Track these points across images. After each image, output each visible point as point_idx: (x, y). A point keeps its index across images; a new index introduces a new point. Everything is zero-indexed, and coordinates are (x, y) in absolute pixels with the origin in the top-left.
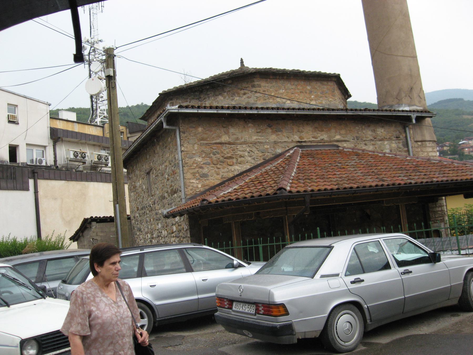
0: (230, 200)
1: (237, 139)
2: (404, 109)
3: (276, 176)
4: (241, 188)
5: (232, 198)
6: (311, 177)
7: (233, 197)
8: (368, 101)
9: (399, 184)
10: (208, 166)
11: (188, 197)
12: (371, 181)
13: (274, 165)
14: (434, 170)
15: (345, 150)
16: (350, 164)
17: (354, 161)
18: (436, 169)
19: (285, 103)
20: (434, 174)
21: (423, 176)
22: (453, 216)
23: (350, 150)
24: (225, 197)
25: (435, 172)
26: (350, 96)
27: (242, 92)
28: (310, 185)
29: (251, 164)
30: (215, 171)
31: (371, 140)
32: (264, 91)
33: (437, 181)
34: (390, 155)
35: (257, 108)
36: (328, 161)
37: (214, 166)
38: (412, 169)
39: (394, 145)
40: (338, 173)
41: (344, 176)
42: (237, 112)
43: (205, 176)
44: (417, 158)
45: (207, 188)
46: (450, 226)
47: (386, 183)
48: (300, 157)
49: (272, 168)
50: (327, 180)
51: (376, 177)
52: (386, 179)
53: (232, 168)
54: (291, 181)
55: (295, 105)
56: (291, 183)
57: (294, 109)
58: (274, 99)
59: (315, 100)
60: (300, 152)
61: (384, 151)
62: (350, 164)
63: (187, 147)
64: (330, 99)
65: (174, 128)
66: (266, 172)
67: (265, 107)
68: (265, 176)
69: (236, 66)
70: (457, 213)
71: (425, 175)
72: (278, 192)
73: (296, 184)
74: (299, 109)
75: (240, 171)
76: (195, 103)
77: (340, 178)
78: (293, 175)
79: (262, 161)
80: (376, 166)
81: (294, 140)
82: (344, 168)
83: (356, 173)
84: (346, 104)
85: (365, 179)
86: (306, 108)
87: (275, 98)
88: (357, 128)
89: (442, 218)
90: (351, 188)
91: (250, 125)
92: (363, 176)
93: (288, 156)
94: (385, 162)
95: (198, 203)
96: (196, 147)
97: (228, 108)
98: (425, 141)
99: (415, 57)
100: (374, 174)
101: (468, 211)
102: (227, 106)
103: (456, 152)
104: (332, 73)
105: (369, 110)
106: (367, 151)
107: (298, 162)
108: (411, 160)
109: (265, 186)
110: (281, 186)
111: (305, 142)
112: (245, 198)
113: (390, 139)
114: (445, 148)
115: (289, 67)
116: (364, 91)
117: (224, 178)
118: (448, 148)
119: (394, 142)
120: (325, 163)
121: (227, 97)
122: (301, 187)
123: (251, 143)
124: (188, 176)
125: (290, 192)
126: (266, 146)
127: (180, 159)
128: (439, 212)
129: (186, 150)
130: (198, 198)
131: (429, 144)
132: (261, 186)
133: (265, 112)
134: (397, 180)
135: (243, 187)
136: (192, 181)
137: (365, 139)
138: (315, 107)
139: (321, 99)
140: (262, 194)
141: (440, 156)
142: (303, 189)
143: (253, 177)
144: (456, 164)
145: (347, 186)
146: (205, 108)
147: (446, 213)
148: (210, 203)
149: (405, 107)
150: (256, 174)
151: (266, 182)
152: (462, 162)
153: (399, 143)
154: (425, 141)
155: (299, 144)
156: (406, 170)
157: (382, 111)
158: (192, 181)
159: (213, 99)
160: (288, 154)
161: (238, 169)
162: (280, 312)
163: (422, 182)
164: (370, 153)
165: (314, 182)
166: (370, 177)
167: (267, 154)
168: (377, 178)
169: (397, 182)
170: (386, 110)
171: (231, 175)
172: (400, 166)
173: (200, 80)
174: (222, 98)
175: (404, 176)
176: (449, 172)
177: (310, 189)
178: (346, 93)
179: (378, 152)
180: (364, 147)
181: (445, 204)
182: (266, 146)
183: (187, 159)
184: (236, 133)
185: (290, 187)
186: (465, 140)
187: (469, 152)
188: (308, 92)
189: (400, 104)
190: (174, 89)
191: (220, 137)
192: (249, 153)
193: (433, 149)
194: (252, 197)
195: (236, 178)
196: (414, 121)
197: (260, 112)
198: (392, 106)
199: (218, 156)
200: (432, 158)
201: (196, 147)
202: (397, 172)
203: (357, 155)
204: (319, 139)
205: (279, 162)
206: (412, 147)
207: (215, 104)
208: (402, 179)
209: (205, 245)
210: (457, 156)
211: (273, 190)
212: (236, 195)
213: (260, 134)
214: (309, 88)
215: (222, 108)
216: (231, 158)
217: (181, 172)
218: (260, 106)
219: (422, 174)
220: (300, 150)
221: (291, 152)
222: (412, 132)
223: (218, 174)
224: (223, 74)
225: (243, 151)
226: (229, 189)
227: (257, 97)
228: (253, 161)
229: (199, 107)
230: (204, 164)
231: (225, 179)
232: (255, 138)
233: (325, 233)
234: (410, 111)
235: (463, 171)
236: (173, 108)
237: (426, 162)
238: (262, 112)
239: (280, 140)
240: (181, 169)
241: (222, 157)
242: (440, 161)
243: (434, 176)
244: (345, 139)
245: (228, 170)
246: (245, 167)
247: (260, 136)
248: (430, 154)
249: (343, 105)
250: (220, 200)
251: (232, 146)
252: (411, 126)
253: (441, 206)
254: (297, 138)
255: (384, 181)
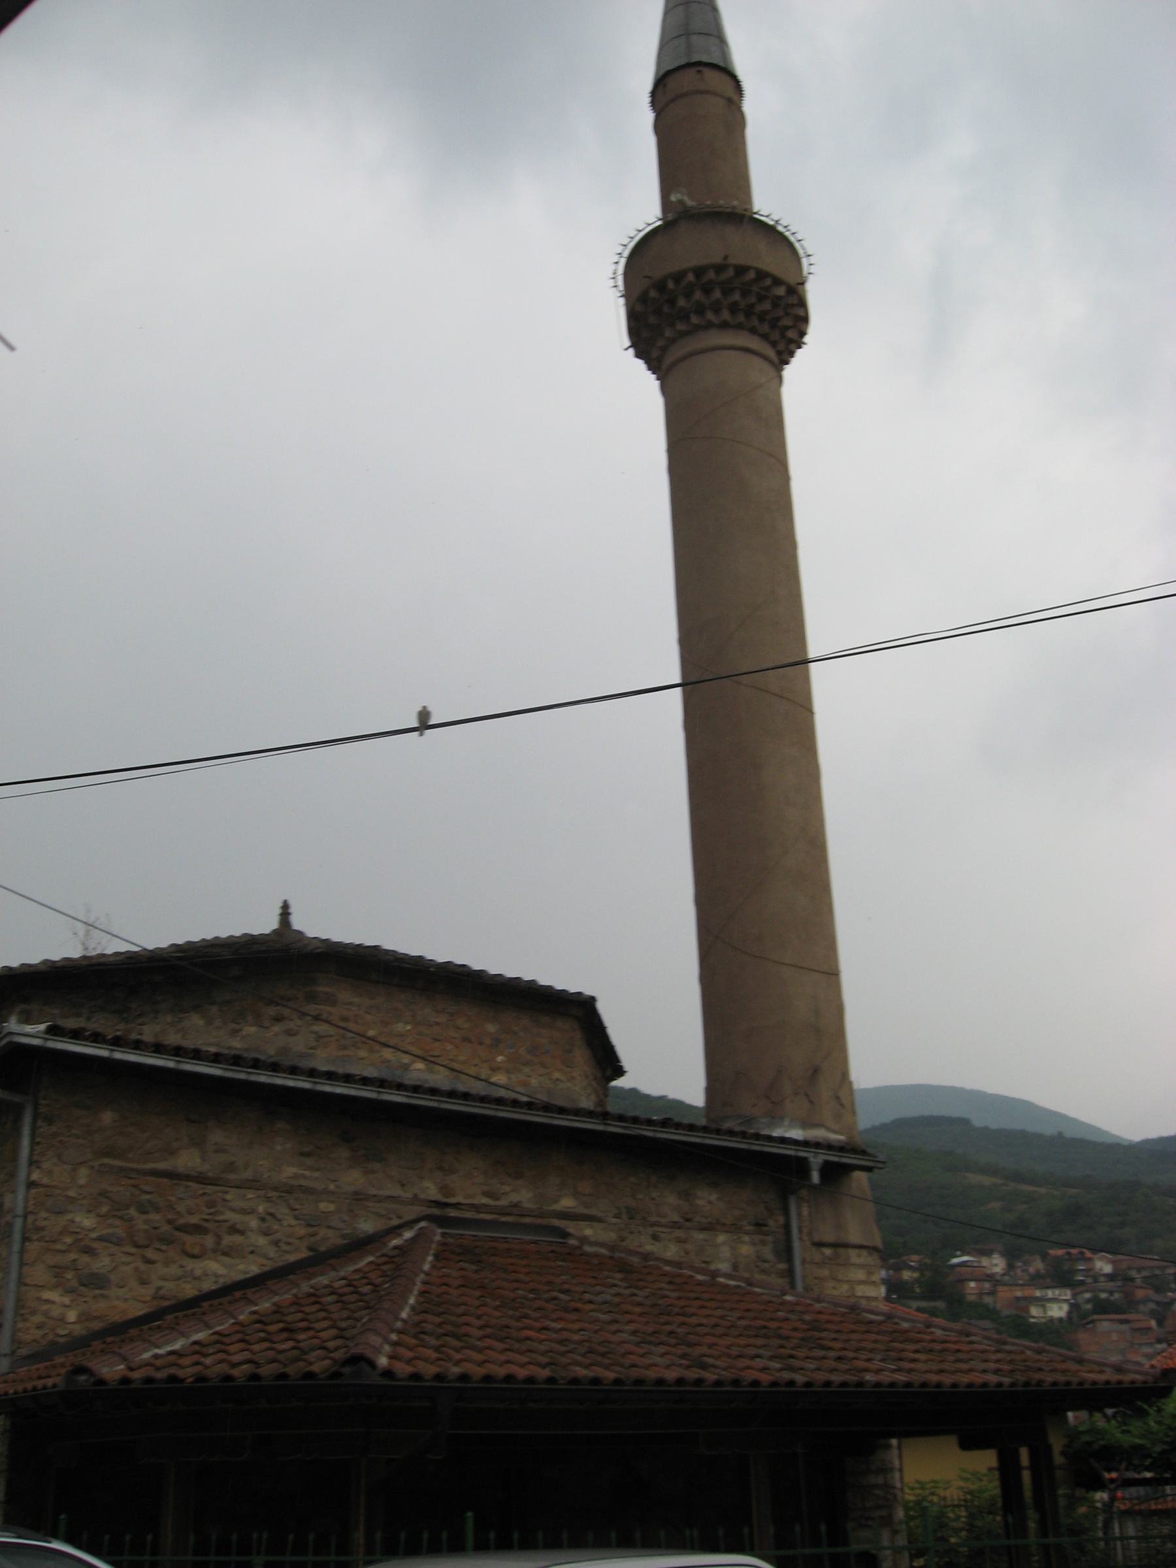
0: (173, 1379)
1: (231, 1167)
2: (787, 1135)
3: (345, 1314)
4: (217, 1342)
5: (180, 1373)
6: (464, 1329)
7: (187, 1372)
8: (673, 1094)
9: (756, 1383)
10: (113, 1249)
11: (24, 1351)
12: (662, 1365)
13: (342, 1274)
14: (870, 1346)
15: (587, 1248)
16: (599, 1299)
17: (614, 1290)
18: (875, 1341)
19: (406, 1067)
20: (869, 1360)
21: (830, 1363)
22: (920, 1508)
23: (603, 1251)
24: (158, 1369)
25: (872, 1351)
26: (619, 1072)
27: (271, 1011)
28: (458, 1356)
29: (264, 1261)
30: (136, 1269)
31: (675, 1225)
32: (345, 1019)
33: (878, 1384)
34: (732, 1283)
35: (312, 1073)
36: (527, 1279)
37: (133, 1250)
38: (799, 1335)
39: (746, 1250)
40: (558, 1326)
41: (576, 1337)
42: (242, 1076)
43: (96, 1282)
44: (818, 1300)
45: (97, 1325)
46: (910, 1542)
47: (711, 1377)
48: (437, 1257)
49: (337, 1284)
50: (517, 1346)
51: (679, 1352)
52: (710, 1361)
53: (197, 1267)
54: (394, 1337)
55: (440, 1078)
56: (395, 1344)
57: (434, 1091)
58: (371, 1051)
59: (508, 1071)
60: (438, 1238)
61: (713, 1267)
62: (599, 1299)
63: (50, 1172)
64: (557, 1075)
65: (16, 1098)
66: (314, 1297)
67: (341, 1071)
68: (307, 1309)
69: (265, 924)
70: (935, 1499)
71: (839, 1358)
72: (347, 1370)
73: (411, 1349)
74: (452, 1094)
75: (221, 1280)
76: (100, 1023)
77: (562, 1342)
78: (404, 1315)
79: (304, 1254)
80: (684, 1315)
81: (422, 1196)
82: (576, 1310)
83: (615, 1333)
84: (606, 1096)
85: (642, 1356)
86: (473, 1092)
87: (377, 1047)
88: (632, 1179)
89: (884, 1513)
90: (596, 1381)
91: (280, 1125)
92: (638, 1344)
93: (396, 1248)
94: (712, 1304)
95: (58, 1380)
96: (83, 1174)
97: (216, 1059)
98: (847, 1246)
99: (833, 974)
100: (673, 1341)
101: (971, 1492)
102: (213, 1049)
103: (940, 1289)
104: (573, 989)
105: (678, 1126)
106: (658, 1259)
107: (427, 1274)
108: (797, 1304)
109: (302, 1345)
110: (357, 1351)
111: (456, 1206)
112: (228, 1378)
113: (734, 1228)
114: (907, 1275)
115: (438, 951)
116: (664, 1055)
117: (163, 1298)
118: (916, 1275)
119: (746, 1238)
120: (515, 1285)
121: (218, 1023)
122: (426, 1360)
123: (276, 1189)
124: (39, 1274)
125: (388, 1373)
126: (324, 1206)
127: (20, 1210)
128: (877, 1492)
129: (45, 1181)
130: (59, 1360)
131: (859, 1256)
132: (290, 1344)
133: (338, 1090)
134: (748, 1368)
135: (227, 1340)
136: (47, 1295)
137: (654, 1219)
138: (502, 1093)
139: (526, 1070)
140: (291, 1370)
141: (887, 1299)
142: (432, 1370)
143: (265, 1305)
144: (939, 1332)
145: (581, 1372)
146: (138, 1046)
147: (899, 1493)
148: (101, 1382)
149: (790, 1127)
150: (276, 1299)
151: (309, 1329)
152: (957, 1326)
153: (763, 1243)
154: (847, 1246)
155: (436, 1211)
156: (780, 1337)
157: (718, 1131)
158: (47, 1295)
159: (169, 1019)
160: (395, 1242)
161: (217, 1271)
162: (681, 1268)
163: (828, 1384)
164: (667, 1268)
165: (474, 1348)
166: (661, 1349)
167: (323, 1232)
168: (684, 1356)
169: (752, 1375)
170: (731, 1133)
171: (189, 1290)
172: (760, 1323)
173: (136, 949)
174: (201, 1022)
175: (772, 1358)
176: (917, 1356)
177: (456, 1370)
178: (607, 1062)
179: (692, 1268)
180: (650, 1247)
181: (897, 1463)
182: (324, 1206)
183: (44, 1214)
184: (225, 1146)
185: (391, 1357)
186: (968, 1254)
187: (980, 1294)
188: (488, 1041)
189: (776, 1118)
190: (44, 968)
191: (172, 1153)
192: (263, 1220)
193: (870, 1273)
194: (255, 1377)
195: (205, 1304)
196: (815, 1177)
197: (320, 1088)
198: (749, 1120)
199: (154, 1217)
200: (864, 1303)
201: (83, 1174)
202: (752, 1341)
203: (624, 1268)
204: (503, 1202)
205: (362, 1264)
206: (804, 1262)
207: (173, 1039)
208: (763, 1368)
209: (55, 1536)
210: (940, 1304)
211: (327, 1362)
212: (197, 1363)
213: (309, 1161)
214: (491, 1028)
215: (197, 1055)
216: (197, 1229)
217: (15, 1258)
218: (324, 1068)
219: (832, 1354)
220: (439, 1231)
221: (408, 1235)
222: (805, 1212)
223: (144, 1282)
224: (216, 944)
225: (244, 1212)
226: (174, 1340)
227: (319, 1037)
228: (272, 1252)
229: (117, 1042)
230: (100, 1239)
231: (167, 1303)
232: (290, 1171)
233: (492, 1535)
234: (806, 1144)
235: (961, 1356)
236: (29, 1029)
237: (843, 1315)
238: (328, 1089)
239: (373, 1191)
240: (16, 1247)
241: (170, 1222)
242: (889, 1317)
243: (867, 1365)
244: (590, 1212)
245: (180, 1272)
246: (241, 1267)
247: (310, 1168)
248: (861, 1290)
249: (593, 1098)
250: (136, 1375)
251: (210, 1189)
252: (804, 1193)
253: (885, 1470)
254: (431, 1190)
255: (704, 1367)
